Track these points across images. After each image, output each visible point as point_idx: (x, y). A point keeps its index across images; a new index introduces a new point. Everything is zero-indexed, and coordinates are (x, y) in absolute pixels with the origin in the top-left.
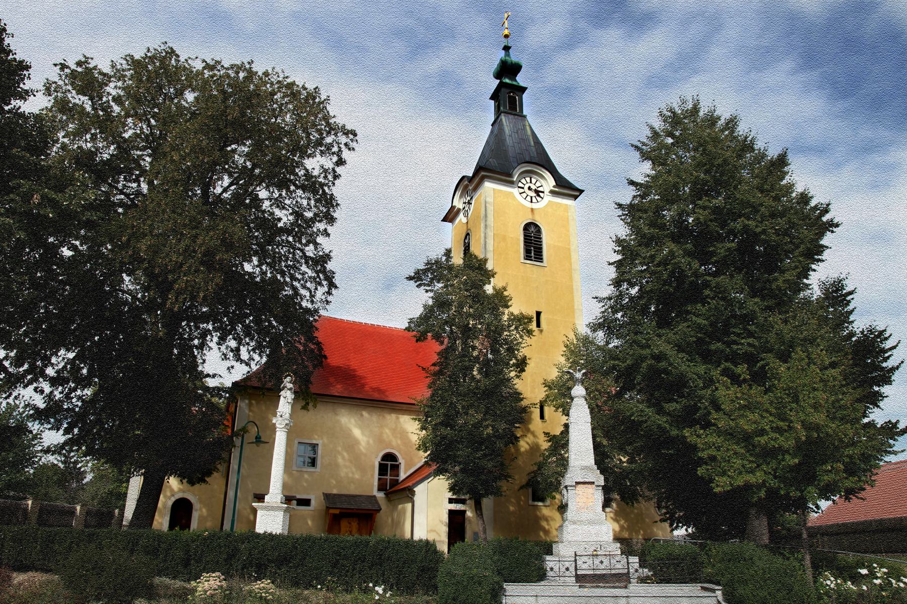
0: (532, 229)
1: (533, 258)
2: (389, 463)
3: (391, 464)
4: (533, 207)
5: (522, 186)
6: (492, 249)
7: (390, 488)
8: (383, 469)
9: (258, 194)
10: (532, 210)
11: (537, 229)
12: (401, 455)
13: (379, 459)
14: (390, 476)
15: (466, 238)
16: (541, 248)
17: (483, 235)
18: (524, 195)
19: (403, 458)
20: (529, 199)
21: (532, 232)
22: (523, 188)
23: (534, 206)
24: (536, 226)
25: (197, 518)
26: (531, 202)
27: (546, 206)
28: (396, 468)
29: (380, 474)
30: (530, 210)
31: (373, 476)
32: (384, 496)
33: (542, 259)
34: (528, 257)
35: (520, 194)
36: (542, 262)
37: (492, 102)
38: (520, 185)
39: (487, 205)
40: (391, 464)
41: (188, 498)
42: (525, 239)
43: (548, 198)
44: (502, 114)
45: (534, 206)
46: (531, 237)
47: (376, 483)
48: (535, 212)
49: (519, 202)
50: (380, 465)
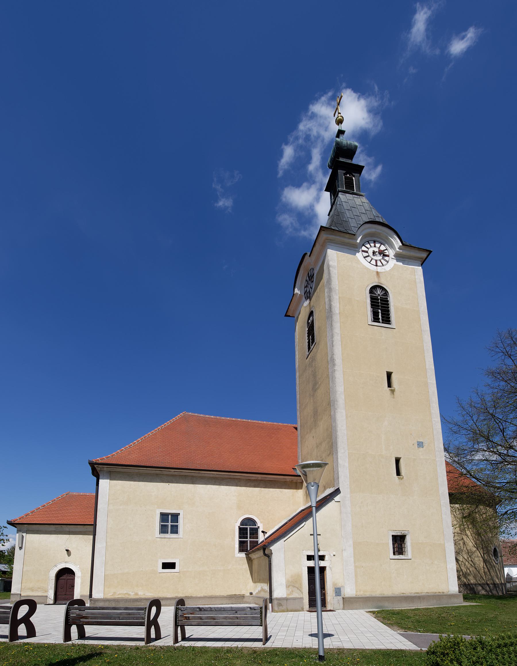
0: (379, 292)
1: (381, 320)
2: (248, 527)
3: (250, 528)
4: (378, 271)
5: (367, 250)
6: (337, 312)
7: (250, 549)
8: (242, 532)
9: (301, 488)
10: (378, 273)
11: (384, 292)
12: (260, 520)
13: (238, 524)
14: (250, 538)
15: (309, 319)
16: (388, 311)
17: (327, 300)
18: (369, 259)
19: (261, 522)
20: (373, 262)
21: (379, 295)
22: (367, 252)
23: (379, 269)
24: (383, 289)
25: (79, 584)
26: (376, 266)
27: (393, 269)
28: (255, 532)
29: (240, 538)
30: (375, 273)
31: (233, 540)
32: (245, 556)
33: (390, 321)
34: (376, 319)
35: (364, 257)
36: (390, 324)
37: (328, 194)
38: (364, 248)
39: (331, 269)
40: (250, 528)
41: (58, 570)
42: (371, 301)
43: (392, 263)
44: (340, 193)
45: (379, 269)
46: (379, 303)
47: (237, 546)
48: (381, 275)
49: (363, 265)
50: (240, 529)
